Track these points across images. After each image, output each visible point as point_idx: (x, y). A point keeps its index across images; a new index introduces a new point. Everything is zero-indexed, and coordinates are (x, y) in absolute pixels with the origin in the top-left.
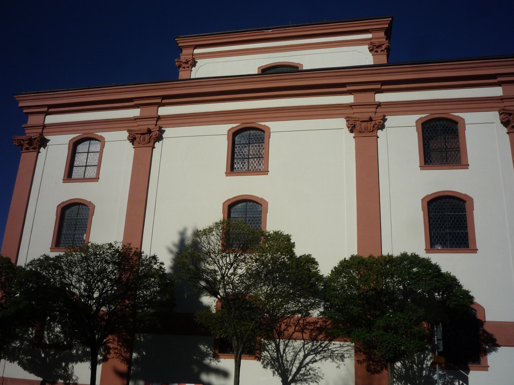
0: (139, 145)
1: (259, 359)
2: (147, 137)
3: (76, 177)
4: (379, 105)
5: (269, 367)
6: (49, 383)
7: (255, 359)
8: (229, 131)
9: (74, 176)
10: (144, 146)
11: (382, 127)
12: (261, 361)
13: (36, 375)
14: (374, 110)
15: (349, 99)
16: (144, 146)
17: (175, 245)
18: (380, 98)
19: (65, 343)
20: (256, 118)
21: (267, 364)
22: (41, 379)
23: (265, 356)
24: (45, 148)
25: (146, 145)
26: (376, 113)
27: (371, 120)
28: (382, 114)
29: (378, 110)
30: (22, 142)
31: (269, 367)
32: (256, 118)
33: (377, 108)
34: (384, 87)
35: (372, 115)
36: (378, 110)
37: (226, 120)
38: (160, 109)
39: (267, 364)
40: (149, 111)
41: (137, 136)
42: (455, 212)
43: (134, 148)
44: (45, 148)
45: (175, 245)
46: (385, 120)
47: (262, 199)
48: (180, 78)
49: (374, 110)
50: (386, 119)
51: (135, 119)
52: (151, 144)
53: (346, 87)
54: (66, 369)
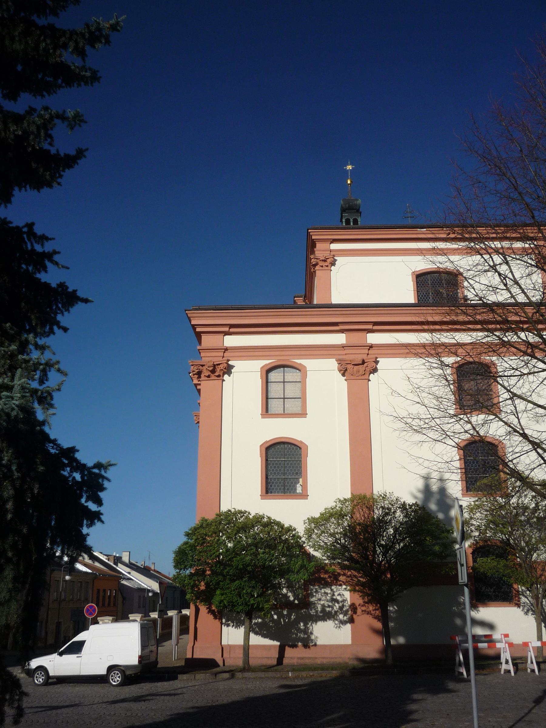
0: (352, 377)
1: (518, 605)
2: (361, 368)
3: (273, 413)
4: (371, 347)
5: (530, 613)
6: (290, 646)
7: (515, 606)
8: (262, 368)
9: (272, 410)
10: (358, 378)
11: (375, 370)
12: (521, 607)
13: (271, 639)
14: (366, 351)
15: (340, 339)
16: (358, 378)
17: (419, 491)
18: (373, 338)
19: (296, 602)
20: (290, 355)
21: (528, 611)
22: (279, 643)
23: (524, 603)
24: (230, 376)
25: (360, 378)
26: (368, 354)
27: (363, 362)
28: (374, 356)
29: (370, 352)
30: (201, 368)
31: (530, 613)
32: (290, 355)
33: (369, 350)
34: (232, 330)
35: (364, 357)
36: (371, 352)
37: (329, 355)
38: (227, 338)
39: (528, 611)
40: (356, 338)
41: (349, 366)
42: (276, 458)
43: (346, 380)
44: (230, 376)
45: (419, 491)
46: (377, 362)
47: (301, 442)
48: (315, 302)
49: (366, 351)
50: (378, 362)
51: (343, 347)
52: (366, 377)
53: (338, 326)
54: (306, 631)
